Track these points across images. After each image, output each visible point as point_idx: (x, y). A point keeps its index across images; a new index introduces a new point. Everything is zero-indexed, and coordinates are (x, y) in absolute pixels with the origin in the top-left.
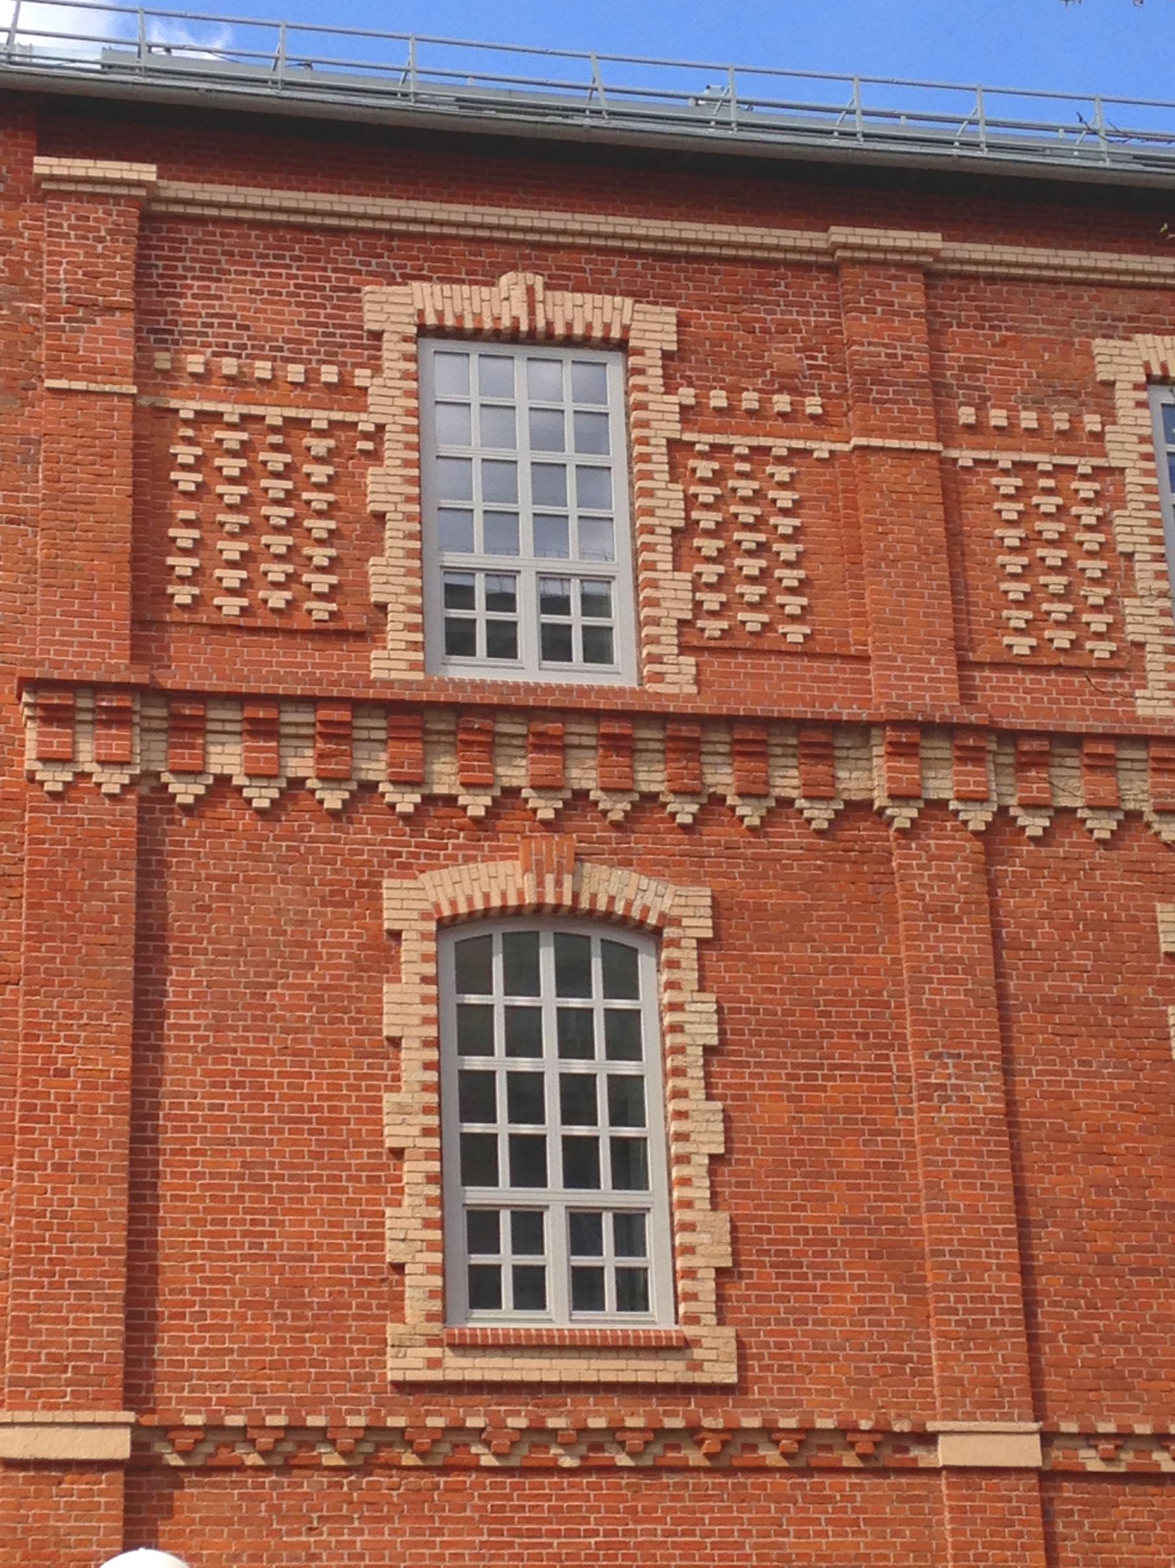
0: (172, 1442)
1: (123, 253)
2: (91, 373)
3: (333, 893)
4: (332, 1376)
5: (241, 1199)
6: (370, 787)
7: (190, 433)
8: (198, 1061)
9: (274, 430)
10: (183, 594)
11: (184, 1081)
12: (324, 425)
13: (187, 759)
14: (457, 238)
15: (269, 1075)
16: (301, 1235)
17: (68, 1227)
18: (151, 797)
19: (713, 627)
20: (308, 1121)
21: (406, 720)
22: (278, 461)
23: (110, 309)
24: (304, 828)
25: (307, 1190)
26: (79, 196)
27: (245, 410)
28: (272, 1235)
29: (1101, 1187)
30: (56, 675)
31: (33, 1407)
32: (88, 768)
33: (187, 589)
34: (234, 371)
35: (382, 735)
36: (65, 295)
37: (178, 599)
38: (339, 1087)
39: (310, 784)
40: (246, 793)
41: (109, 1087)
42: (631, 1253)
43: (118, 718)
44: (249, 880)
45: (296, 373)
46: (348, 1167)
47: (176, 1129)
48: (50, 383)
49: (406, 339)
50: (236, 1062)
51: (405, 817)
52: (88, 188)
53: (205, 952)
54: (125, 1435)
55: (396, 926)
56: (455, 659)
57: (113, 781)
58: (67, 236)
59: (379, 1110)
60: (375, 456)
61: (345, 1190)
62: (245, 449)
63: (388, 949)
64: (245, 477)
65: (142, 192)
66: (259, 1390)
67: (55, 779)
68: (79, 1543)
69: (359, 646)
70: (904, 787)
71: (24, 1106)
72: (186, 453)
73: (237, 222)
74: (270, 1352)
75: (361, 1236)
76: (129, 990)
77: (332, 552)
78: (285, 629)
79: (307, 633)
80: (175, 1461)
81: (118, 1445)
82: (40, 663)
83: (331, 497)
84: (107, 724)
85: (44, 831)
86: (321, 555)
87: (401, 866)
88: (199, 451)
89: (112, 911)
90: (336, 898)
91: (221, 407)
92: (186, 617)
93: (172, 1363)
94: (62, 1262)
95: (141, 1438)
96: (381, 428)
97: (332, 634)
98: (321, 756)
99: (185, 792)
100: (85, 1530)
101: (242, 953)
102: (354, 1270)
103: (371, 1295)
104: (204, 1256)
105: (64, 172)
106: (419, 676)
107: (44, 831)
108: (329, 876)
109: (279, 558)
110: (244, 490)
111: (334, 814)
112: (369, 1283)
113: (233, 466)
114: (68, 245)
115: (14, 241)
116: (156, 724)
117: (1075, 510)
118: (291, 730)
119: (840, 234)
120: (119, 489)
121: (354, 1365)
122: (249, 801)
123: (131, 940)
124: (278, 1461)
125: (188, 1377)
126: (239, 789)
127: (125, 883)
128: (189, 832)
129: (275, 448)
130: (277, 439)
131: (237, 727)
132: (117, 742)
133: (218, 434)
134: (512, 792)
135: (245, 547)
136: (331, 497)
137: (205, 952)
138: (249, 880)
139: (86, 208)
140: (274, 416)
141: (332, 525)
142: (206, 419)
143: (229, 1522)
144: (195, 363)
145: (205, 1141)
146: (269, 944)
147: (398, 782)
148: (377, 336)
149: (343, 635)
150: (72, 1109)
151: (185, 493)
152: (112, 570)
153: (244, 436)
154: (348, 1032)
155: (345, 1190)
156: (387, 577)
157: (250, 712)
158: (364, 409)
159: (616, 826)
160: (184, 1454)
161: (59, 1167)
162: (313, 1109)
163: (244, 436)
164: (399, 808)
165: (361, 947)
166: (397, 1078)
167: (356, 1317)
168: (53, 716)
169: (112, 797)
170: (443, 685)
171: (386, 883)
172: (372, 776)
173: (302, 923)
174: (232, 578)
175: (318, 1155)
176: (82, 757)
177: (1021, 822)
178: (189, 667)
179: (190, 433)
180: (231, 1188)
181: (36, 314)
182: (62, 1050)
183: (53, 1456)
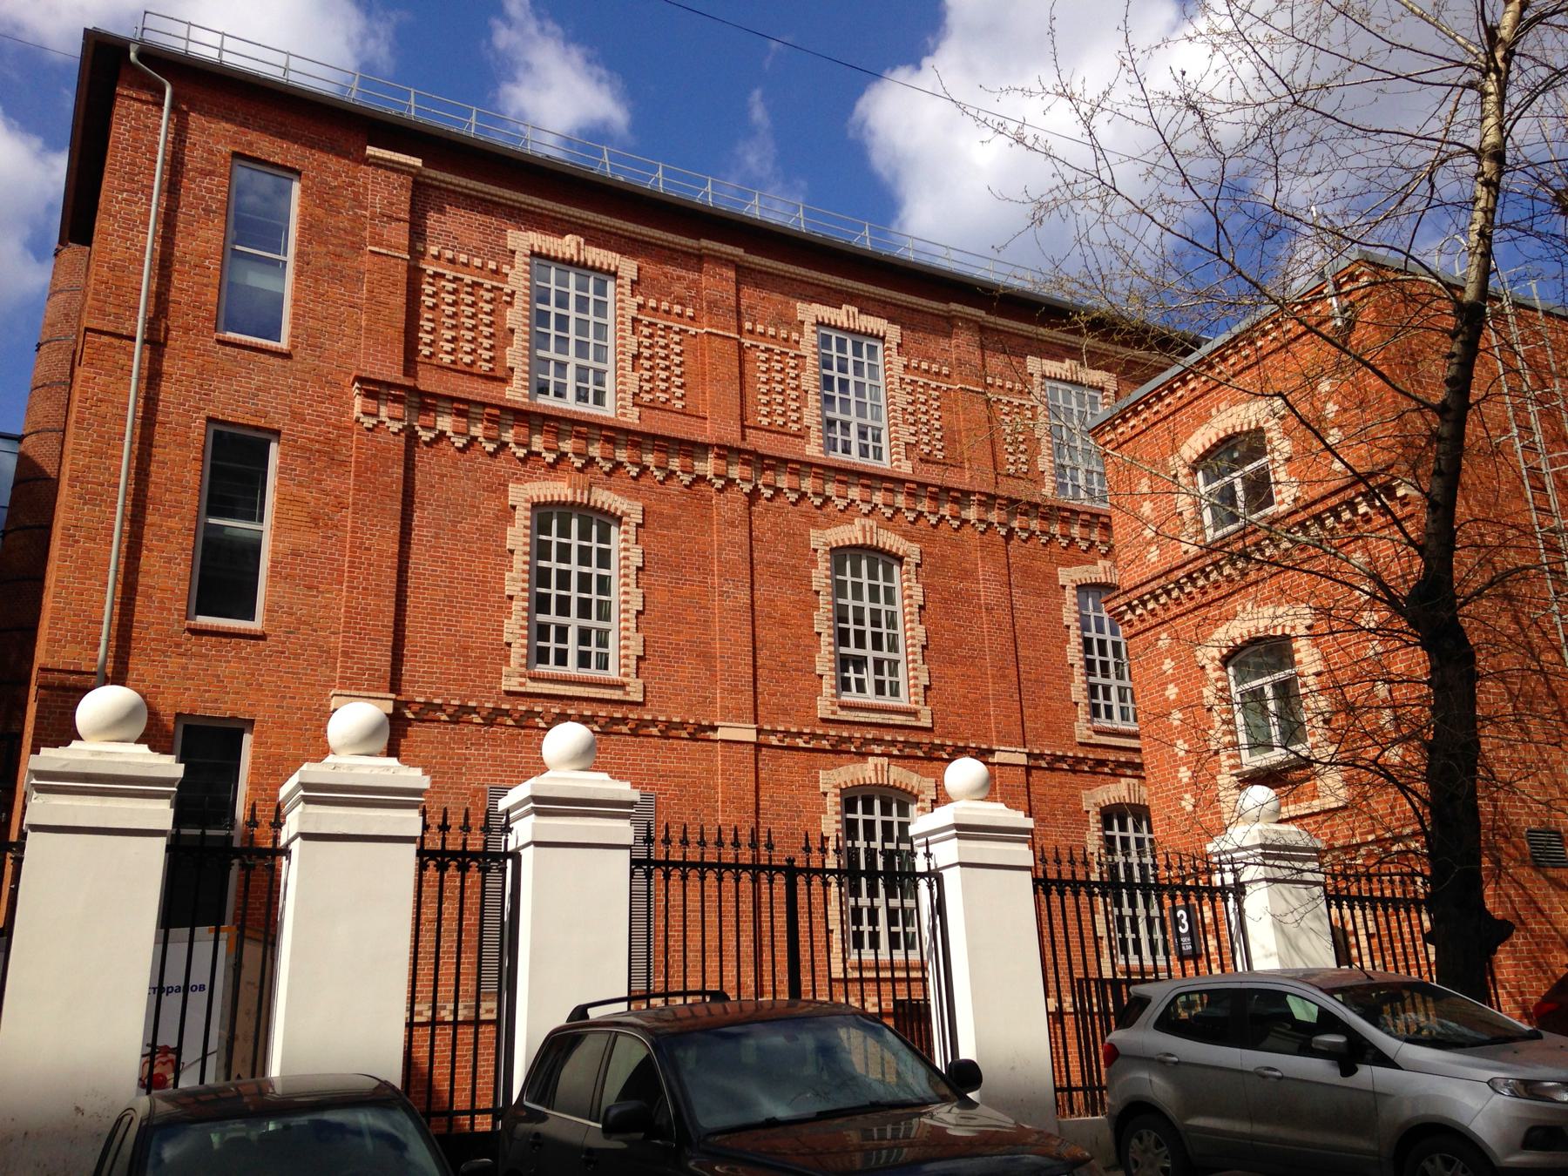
2: (389, 247)
19: (647, 397)
29: (784, 637)
119: (704, 243)
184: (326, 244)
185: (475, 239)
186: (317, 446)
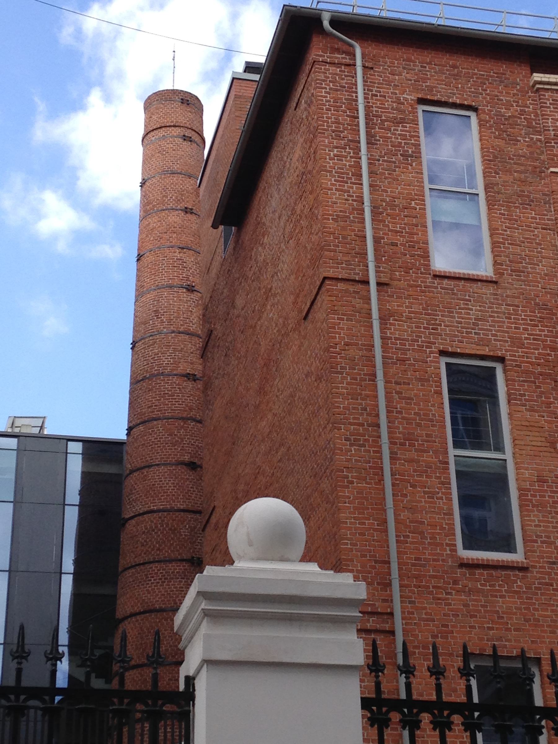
36: (553, 133)
42: (478, 443)
48: (552, 169)
58: (549, 107)
105: (547, 80)
114: (550, 111)
115: (527, 109)
181: (540, 140)
184: (509, 171)
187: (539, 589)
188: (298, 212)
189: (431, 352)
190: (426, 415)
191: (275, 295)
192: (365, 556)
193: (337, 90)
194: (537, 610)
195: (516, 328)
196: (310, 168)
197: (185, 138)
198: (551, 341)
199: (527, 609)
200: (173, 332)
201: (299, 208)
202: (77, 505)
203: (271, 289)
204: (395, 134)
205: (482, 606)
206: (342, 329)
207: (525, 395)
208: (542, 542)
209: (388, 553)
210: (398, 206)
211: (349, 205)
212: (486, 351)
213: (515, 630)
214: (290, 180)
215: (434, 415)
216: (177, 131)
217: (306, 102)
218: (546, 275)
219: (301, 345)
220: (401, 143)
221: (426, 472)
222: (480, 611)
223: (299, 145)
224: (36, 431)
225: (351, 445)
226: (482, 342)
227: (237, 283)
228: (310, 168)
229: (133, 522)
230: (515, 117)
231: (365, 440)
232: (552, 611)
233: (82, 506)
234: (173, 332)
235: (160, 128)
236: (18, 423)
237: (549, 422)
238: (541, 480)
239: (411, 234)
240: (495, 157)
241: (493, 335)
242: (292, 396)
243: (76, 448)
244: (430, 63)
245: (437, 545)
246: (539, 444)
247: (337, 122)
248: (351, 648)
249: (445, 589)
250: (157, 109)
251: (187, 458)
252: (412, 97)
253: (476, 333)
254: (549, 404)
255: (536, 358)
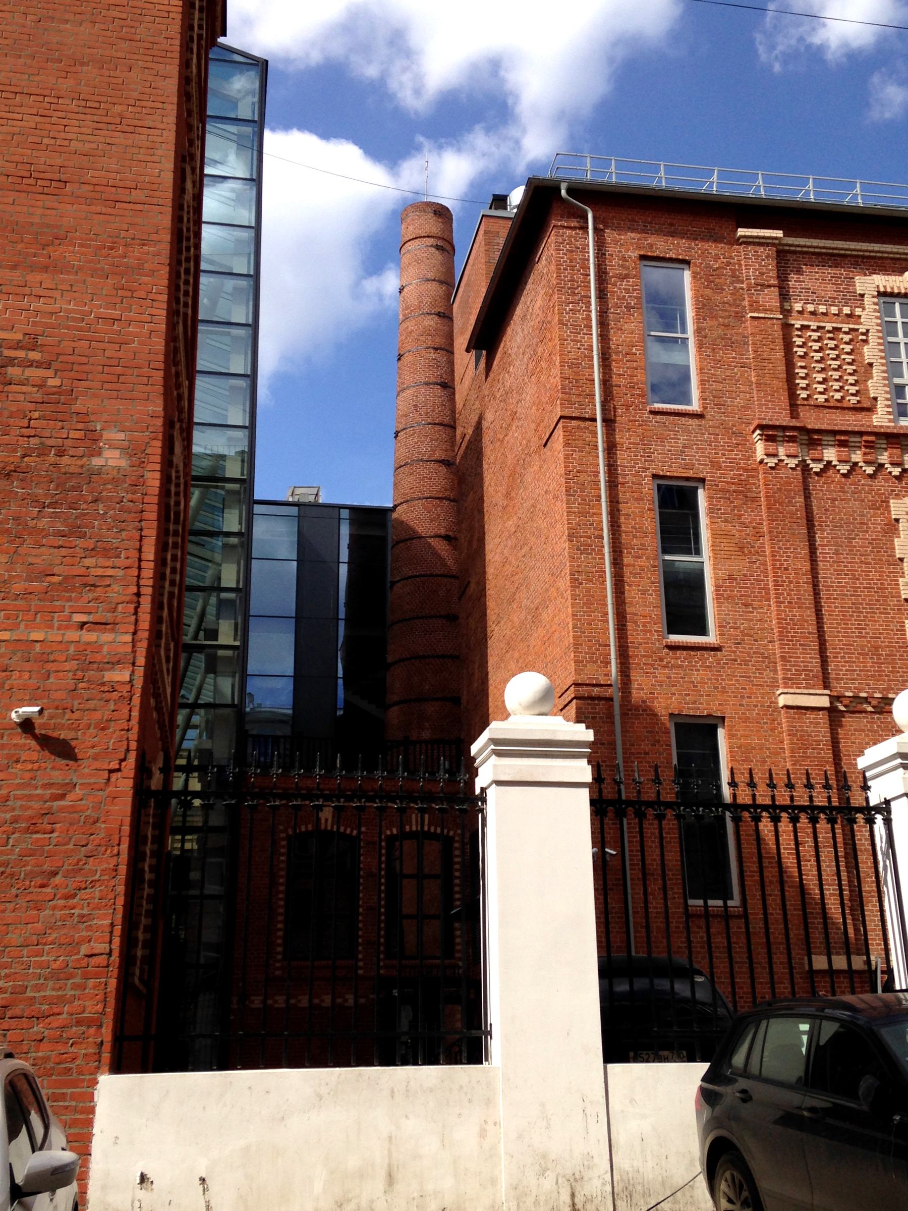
0: (841, 702)
1: (772, 265)
3: (873, 505)
4: (894, 680)
5: (852, 616)
6: (882, 466)
7: (799, 333)
8: (831, 566)
9: (829, 332)
10: (804, 394)
11: (826, 571)
12: (847, 330)
13: (815, 454)
14: (887, 258)
15: (857, 571)
16: (876, 629)
17: (795, 624)
18: (805, 468)
20: (873, 588)
21: (894, 441)
22: (832, 344)
23: (769, 286)
24: (859, 481)
25: (876, 613)
26: (754, 244)
27: (819, 324)
28: (865, 629)
30: (771, 423)
31: (792, 688)
32: (783, 458)
33: (805, 392)
34: (812, 309)
35: (885, 446)
37: (802, 396)
38: (882, 576)
39: (860, 464)
40: (838, 468)
41: (803, 574)
43: (792, 439)
44: (842, 500)
45: (834, 310)
46: (889, 605)
47: (827, 590)
49: (873, 297)
50: (845, 566)
51: (896, 477)
52: (757, 240)
53: (828, 526)
54: (827, 699)
55: (898, 517)
56: (901, 418)
57: (792, 463)
59: (898, 585)
60: (866, 341)
61: (889, 614)
62: (819, 339)
63: (894, 526)
64: (821, 349)
65: (777, 242)
66: (868, 685)
67: (772, 462)
68: (816, 736)
69: (868, 413)
70: (844, 458)
71: (774, 581)
72: (799, 341)
73: (807, 253)
74: (870, 671)
75: (897, 630)
76: (806, 539)
77: (855, 378)
78: (840, 407)
79: (849, 409)
80: (843, 709)
81: (825, 702)
82: (765, 419)
83: (852, 357)
84: (788, 442)
85: (770, 481)
86: (851, 379)
87: (896, 495)
88: (803, 340)
89: (797, 510)
90: (874, 507)
91: (810, 323)
92: (806, 403)
93: (836, 674)
94: (795, 637)
95: (834, 699)
96: (868, 331)
97: (857, 409)
98: (865, 454)
99: (816, 467)
100: (817, 731)
101: (842, 527)
102: (897, 643)
103: (904, 652)
104: (843, 636)
106: (892, 424)
107: (770, 481)
108: (870, 498)
109: (836, 380)
110: (821, 355)
111: (870, 476)
112: (902, 647)
113: (816, 346)
116: (804, 442)
117: (842, 347)
118: (853, 444)
120: (780, 355)
121: (901, 676)
122: (839, 471)
123: (805, 521)
124: (879, 710)
125: (842, 679)
126: (835, 466)
127: (800, 500)
128: (818, 482)
129: (830, 339)
130: (831, 335)
131: (832, 443)
132: (793, 448)
133: (809, 334)
134: (856, 464)
135: (824, 376)
136: (852, 357)
137: (828, 526)
138: (842, 500)
139: (757, 248)
140: (829, 327)
141: (854, 367)
142: (804, 328)
143: (864, 731)
144: (798, 307)
145: (837, 595)
146: (851, 523)
147: (893, 464)
148: (862, 296)
149: (862, 409)
150: (790, 582)
151: (800, 356)
152: (780, 384)
153: (819, 334)
154: (883, 556)
155: (889, 614)
156: (876, 386)
157: (838, 437)
158: (861, 324)
159: (844, 475)
160: (845, 706)
161: (790, 603)
162: (875, 584)
163: (819, 334)
164: (893, 474)
165: (885, 525)
166: (903, 573)
167: (899, 659)
168: (769, 439)
169: (792, 468)
170: (901, 427)
171: (891, 501)
172: (882, 462)
173: (863, 515)
174: (821, 388)
175: (878, 601)
176: (780, 454)
177: (811, 466)
178: (811, 420)
179: (799, 333)
180: (848, 612)
182: (785, 561)
183: (803, 705)
184: (713, 317)
185: (829, 290)
186: (734, 487)
187: (727, 664)
188: (539, 354)
189: (645, 476)
190: (641, 528)
191: (519, 419)
192: (591, 641)
193: (572, 252)
194: (724, 680)
195: (716, 453)
196: (549, 318)
197: (438, 248)
198: (744, 464)
199: (717, 679)
200: (430, 424)
201: (540, 350)
202: (205, 222)
203: (516, 413)
204: (620, 289)
205: (682, 678)
206: (575, 459)
207: (720, 509)
208: (730, 627)
209: (609, 638)
210: (621, 352)
211: (582, 353)
212: (690, 474)
213: (707, 695)
214: (532, 324)
215: (647, 528)
216: (431, 241)
217: (546, 260)
218: (743, 407)
219: (541, 467)
220: (624, 296)
221: (640, 574)
222: (679, 682)
223: (540, 295)
224: (312, 499)
225: (581, 554)
226: (687, 467)
227: (487, 399)
228: (549, 318)
229: (399, 585)
230: (723, 268)
231: (592, 550)
232: (736, 680)
233: (349, 563)
234: (430, 424)
235: (416, 238)
236: (298, 491)
237: (740, 531)
238: (731, 578)
239: (632, 376)
240: (704, 305)
241: (697, 460)
242: (534, 506)
243: (345, 513)
244: (651, 223)
245: (646, 631)
246: (731, 549)
247: (572, 280)
248: (582, 771)
249: (652, 665)
250: (413, 220)
251: (443, 532)
252: (634, 254)
253: (683, 459)
254: (740, 516)
255: (731, 478)
